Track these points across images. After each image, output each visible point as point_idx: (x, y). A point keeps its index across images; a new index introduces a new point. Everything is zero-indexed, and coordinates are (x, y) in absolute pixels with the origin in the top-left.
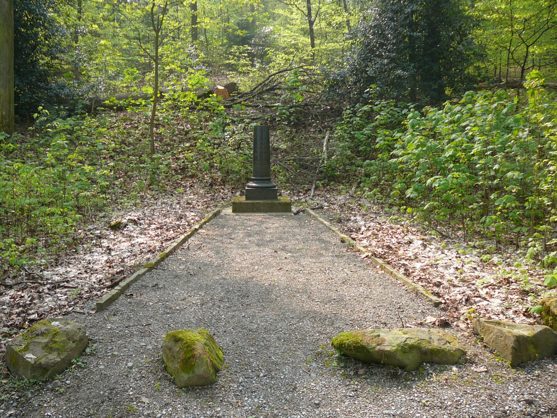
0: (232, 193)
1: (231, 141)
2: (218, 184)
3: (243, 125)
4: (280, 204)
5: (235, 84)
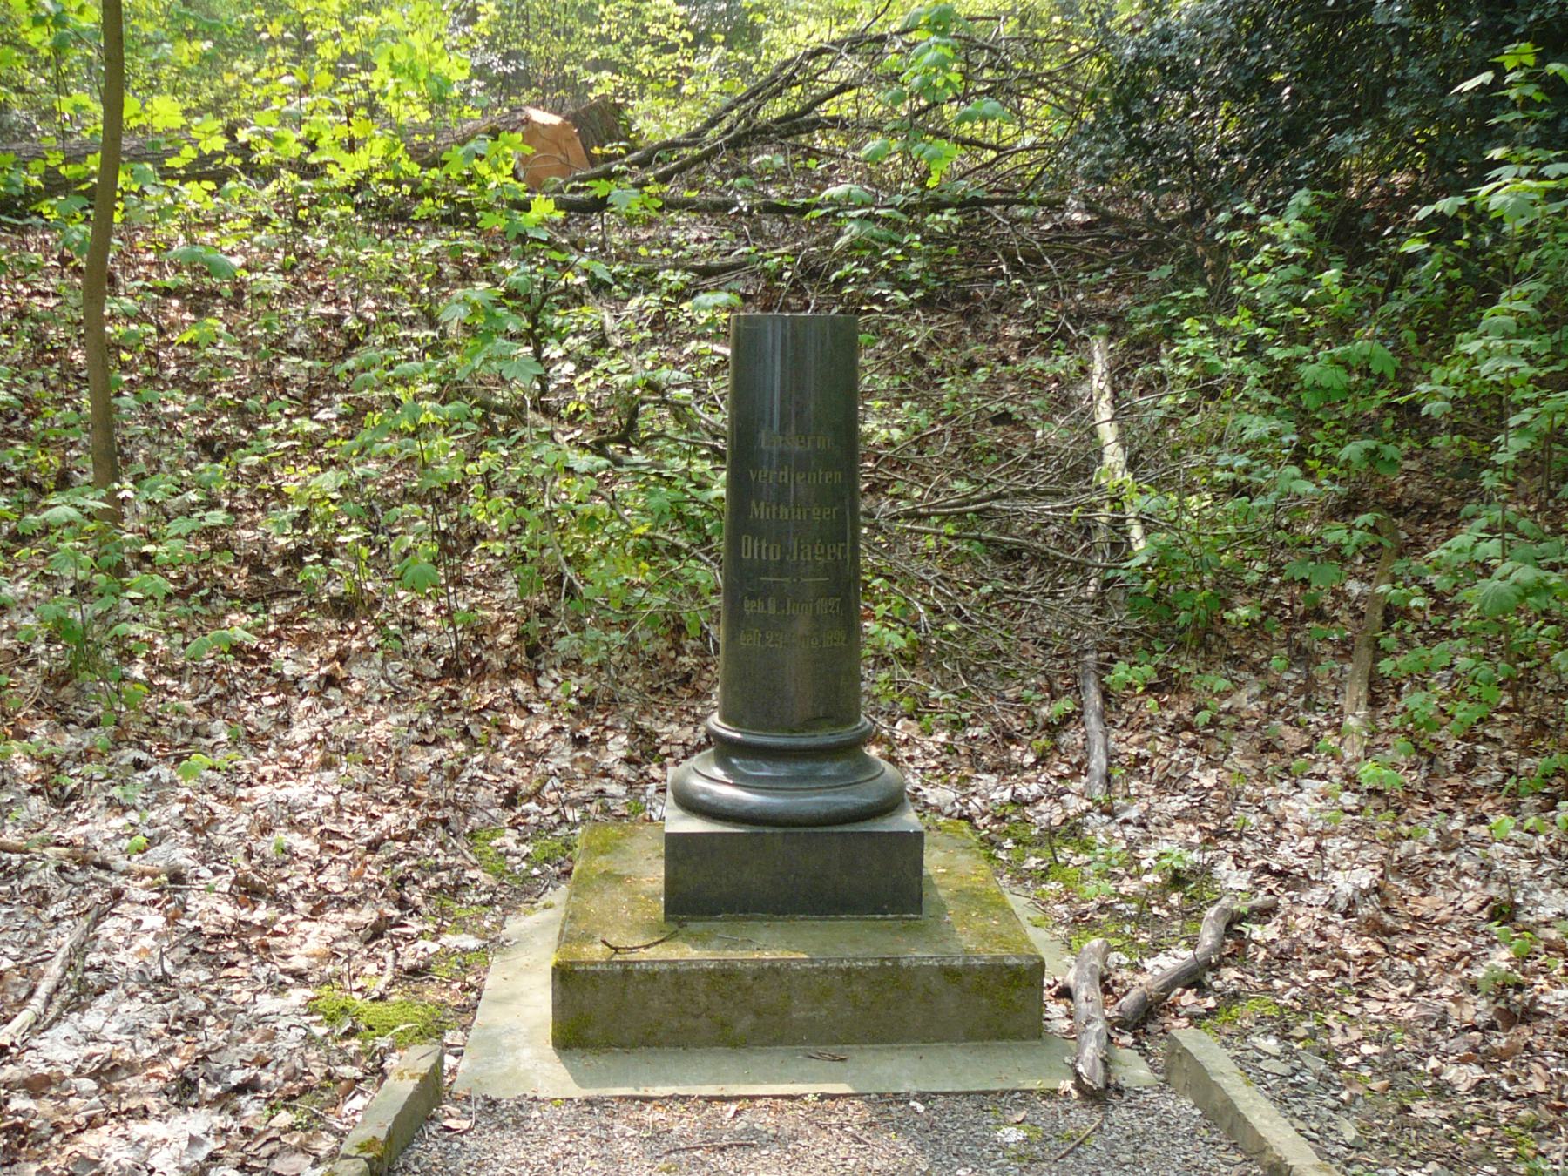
0: (580, 742)
1: (586, 388)
2: (499, 663)
3: (653, 300)
5: (619, 108)
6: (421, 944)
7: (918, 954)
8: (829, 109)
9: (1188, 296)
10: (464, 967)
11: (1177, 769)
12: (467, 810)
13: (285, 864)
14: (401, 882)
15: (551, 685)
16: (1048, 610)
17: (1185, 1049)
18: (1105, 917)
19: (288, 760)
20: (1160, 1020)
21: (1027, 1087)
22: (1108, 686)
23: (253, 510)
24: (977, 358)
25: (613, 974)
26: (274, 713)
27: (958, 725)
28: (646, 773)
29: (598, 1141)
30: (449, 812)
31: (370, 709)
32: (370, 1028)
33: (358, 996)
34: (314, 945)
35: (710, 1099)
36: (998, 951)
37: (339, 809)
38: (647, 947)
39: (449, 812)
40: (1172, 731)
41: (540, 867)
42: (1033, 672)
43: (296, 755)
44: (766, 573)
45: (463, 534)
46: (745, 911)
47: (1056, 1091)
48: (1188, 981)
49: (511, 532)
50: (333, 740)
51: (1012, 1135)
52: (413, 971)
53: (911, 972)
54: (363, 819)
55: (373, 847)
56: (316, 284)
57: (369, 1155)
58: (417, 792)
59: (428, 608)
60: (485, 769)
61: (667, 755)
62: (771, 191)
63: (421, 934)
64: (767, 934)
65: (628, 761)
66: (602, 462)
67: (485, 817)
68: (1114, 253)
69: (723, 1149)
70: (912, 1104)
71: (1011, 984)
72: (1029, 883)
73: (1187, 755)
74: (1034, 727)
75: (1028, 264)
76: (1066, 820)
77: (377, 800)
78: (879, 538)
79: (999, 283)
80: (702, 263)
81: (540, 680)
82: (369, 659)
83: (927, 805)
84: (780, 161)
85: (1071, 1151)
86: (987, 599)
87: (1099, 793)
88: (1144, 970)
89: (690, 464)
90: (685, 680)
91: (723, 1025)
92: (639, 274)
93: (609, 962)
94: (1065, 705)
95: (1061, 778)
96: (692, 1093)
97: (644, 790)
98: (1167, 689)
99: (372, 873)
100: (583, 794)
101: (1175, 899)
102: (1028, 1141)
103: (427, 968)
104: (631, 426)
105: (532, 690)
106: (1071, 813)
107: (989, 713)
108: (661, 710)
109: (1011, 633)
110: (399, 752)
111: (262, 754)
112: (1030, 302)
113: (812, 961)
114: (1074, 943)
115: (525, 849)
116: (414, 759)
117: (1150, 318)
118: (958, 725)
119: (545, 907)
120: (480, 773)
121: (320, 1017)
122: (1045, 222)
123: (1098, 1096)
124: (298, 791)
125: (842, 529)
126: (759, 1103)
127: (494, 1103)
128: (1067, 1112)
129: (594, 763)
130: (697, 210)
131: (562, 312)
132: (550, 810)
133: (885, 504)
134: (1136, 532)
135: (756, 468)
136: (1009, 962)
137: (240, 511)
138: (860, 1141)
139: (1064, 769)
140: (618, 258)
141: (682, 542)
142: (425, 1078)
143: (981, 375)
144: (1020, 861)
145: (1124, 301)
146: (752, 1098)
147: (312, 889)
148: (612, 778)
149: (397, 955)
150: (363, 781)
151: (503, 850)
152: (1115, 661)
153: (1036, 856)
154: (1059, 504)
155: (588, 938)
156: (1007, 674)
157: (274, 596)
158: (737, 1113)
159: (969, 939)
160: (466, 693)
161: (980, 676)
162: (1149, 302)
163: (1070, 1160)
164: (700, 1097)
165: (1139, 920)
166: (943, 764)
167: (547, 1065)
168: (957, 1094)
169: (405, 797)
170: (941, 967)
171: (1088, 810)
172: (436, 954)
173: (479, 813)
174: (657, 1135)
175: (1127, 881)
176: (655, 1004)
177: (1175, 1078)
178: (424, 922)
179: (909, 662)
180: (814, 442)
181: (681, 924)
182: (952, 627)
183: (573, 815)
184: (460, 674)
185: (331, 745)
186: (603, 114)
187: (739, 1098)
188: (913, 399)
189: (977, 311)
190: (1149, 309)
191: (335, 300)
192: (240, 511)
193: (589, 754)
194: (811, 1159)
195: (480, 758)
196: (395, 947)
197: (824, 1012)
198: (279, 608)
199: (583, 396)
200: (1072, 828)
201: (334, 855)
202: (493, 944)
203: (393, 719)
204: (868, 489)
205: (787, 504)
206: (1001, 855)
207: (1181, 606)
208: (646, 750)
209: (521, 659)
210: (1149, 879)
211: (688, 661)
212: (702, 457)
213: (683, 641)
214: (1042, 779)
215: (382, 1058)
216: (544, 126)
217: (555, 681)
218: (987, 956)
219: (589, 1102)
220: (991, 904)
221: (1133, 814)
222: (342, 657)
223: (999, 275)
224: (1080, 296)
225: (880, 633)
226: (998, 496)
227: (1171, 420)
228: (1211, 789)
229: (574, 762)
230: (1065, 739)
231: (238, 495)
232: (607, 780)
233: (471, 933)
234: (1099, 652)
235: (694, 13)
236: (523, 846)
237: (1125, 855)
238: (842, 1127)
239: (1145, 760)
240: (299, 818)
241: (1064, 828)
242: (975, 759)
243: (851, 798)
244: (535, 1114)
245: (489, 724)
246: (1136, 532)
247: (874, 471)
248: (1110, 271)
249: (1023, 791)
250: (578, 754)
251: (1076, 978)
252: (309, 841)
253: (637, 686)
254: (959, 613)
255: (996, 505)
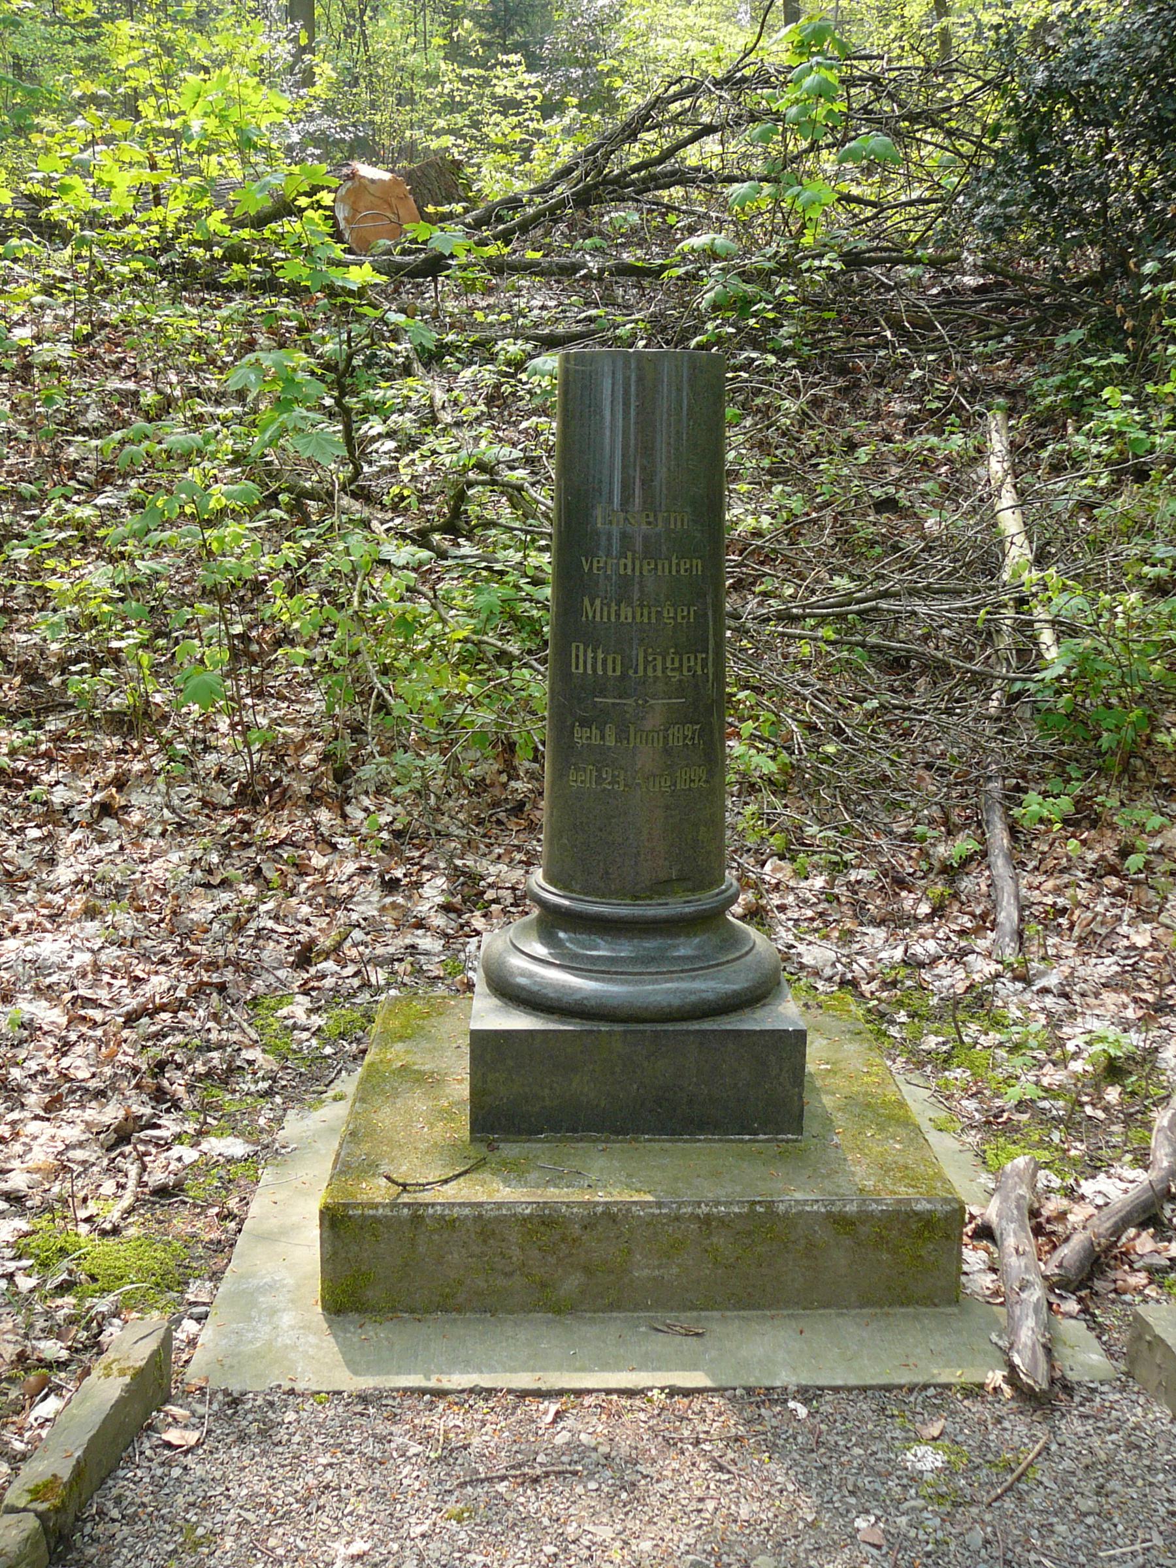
1: (412, 466)
3: (488, 375)
4: (841, 1222)
5: (457, 165)
6: (177, 1151)
7: (798, 1196)
8: (692, 156)
9: (1104, 363)
10: (227, 1184)
11: (1103, 923)
12: (249, 972)
13: (22, 1042)
14: (160, 1067)
15: (362, 815)
16: (944, 730)
17: (1156, 1337)
18: (1025, 1117)
19: (48, 905)
20: (1112, 1275)
21: (943, 1379)
22: (1016, 821)
23: (31, 611)
24: (857, 438)
25: (398, 1220)
26: (39, 848)
27: (838, 868)
28: (468, 924)
29: (371, 1464)
30: (229, 975)
31: (148, 843)
32: (93, 1278)
33: (84, 1228)
34: (41, 1156)
35: (523, 1394)
36: (904, 1192)
37: (97, 969)
38: (446, 1182)
39: (229, 975)
40: (1094, 875)
41: (334, 1044)
42: (928, 804)
43: (58, 899)
44: (603, 693)
45: (267, 637)
46: (575, 1130)
47: (981, 1386)
48: (1143, 1218)
49: (322, 635)
50: (102, 881)
51: (927, 1459)
52: (162, 1192)
53: (790, 1220)
54: (125, 982)
55: (131, 1019)
56: (114, 357)
57: (42, 1507)
58: (193, 948)
59: (223, 724)
60: (276, 918)
61: (494, 901)
62: (625, 255)
63: (178, 1137)
64: (601, 1162)
65: (446, 908)
66: (425, 554)
67: (272, 979)
68: (1012, 319)
69: (536, 1480)
70: (792, 1404)
71: (920, 1234)
72: (929, 1068)
73: (1113, 905)
74: (931, 870)
75: (916, 331)
76: (971, 987)
77: (144, 957)
78: (744, 642)
79: (882, 353)
80: (547, 331)
81: (348, 809)
82: (152, 784)
83: (802, 967)
84: (635, 218)
85: (1009, 1489)
86: (870, 715)
87: (1010, 954)
88: (1083, 1197)
89: (525, 557)
90: (518, 809)
91: (544, 1285)
92: (475, 344)
93: (394, 1205)
94: (964, 844)
95: (962, 933)
96: (499, 1385)
97: (465, 944)
98: (1085, 823)
99: (126, 1056)
100: (391, 950)
101: (1113, 1094)
102: (949, 1470)
103: (179, 1187)
104: (456, 512)
105: (339, 821)
106: (977, 977)
107: (877, 851)
108: (489, 846)
109: (900, 755)
110: (177, 897)
111: (20, 898)
112: (917, 373)
113: (659, 1205)
114: (990, 1155)
115: (317, 1021)
116: (195, 904)
117: (1059, 389)
118: (838, 868)
119: (335, 1099)
120: (270, 924)
121: (31, 1262)
122: (933, 286)
123: (1043, 1398)
124: (50, 947)
125: (702, 634)
126: (588, 1400)
127: (235, 1402)
128: (999, 1420)
129: (406, 911)
130: (542, 274)
131: (383, 384)
132: (351, 970)
133: (753, 603)
134: (1047, 637)
135: (591, 554)
136: (918, 1207)
137: (16, 612)
138: (721, 1468)
139: (966, 922)
140: (452, 326)
141: (513, 648)
142: (140, 1375)
143: (863, 454)
144: (917, 1039)
145: (1025, 372)
146: (579, 1393)
147: (53, 1074)
148: (428, 929)
149: (144, 1168)
150: (130, 933)
151: (290, 1022)
152: (1025, 791)
153: (936, 1033)
154: (959, 604)
155: (369, 1168)
156: (895, 804)
157: (48, 710)
158: (559, 1415)
159: (863, 1172)
160: (261, 826)
161: (864, 806)
162: (1052, 374)
163: (1009, 1504)
164: (510, 1391)
165: (1071, 1123)
166: (821, 914)
167: (312, 1339)
168: (850, 1389)
169: (179, 954)
170: (829, 1214)
171: (998, 975)
172: (193, 1164)
173: (265, 975)
174: (450, 1454)
175: (1049, 1068)
176: (455, 1257)
177: (1141, 1371)
178: (183, 1120)
179: (779, 788)
180: (667, 520)
181: (492, 1147)
182: (831, 749)
183: (378, 976)
184: (256, 801)
185: (99, 888)
186: (441, 173)
187: (561, 1393)
188: (785, 483)
189: (856, 385)
190: (1056, 380)
191: (135, 375)
192: (16, 612)
193: (401, 900)
194: (654, 1500)
195: (271, 905)
196: (142, 1156)
197: (675, 1270)
198: (53, 724)
199: (406, 479)
200: (979, 998)
201: (84, 1029)
202: (266, 1151)
203: (174, 857)
204: (732, 586)
205: (630, 604)
206: (893, 1031)
207: (1104, 725)
208: (469, 895)
209: (328, 783)
210: (1077, 1066)
211: (521, 786)
212: (541, 549)
213: (516, 762)
214: (941, 935)
215: (99, 1325)
216: (373, 181)
217: (366, 810)
218: (889, 1199)
219: (364, 1399)
220: (890, 1118)
221: (1052, 980)
222: (120, 783)
223: (886, 344)
224: (974, 368)
225: (744, 754)
226: (885, 595)
227: (1086, 507)
228: (1145, 949)
229: (383, 909)
230: (966, 884)
231: (15, 594)
232: (420, 932)
233: (241, 1134)
234: (1004, 778)
235: (547, 80)
236: (314, 1017)
237: (1045, 1034)
238: (697, 1442)
239: (1063, 911)
240: (48, 981)
241: (969, 998)
242: (858, 909)
243: (712, 984)
244: (290, 1416)
245: (286, 863)
246: (1047, 637)
247: (740, 565)
248: (1008, 339)
249: (917, 949)
250: (388, 900)
251: (1000, 1216)
252: (57, 1011)
253: (461, 816)
254: (839, 731)
255: (883, 604)
